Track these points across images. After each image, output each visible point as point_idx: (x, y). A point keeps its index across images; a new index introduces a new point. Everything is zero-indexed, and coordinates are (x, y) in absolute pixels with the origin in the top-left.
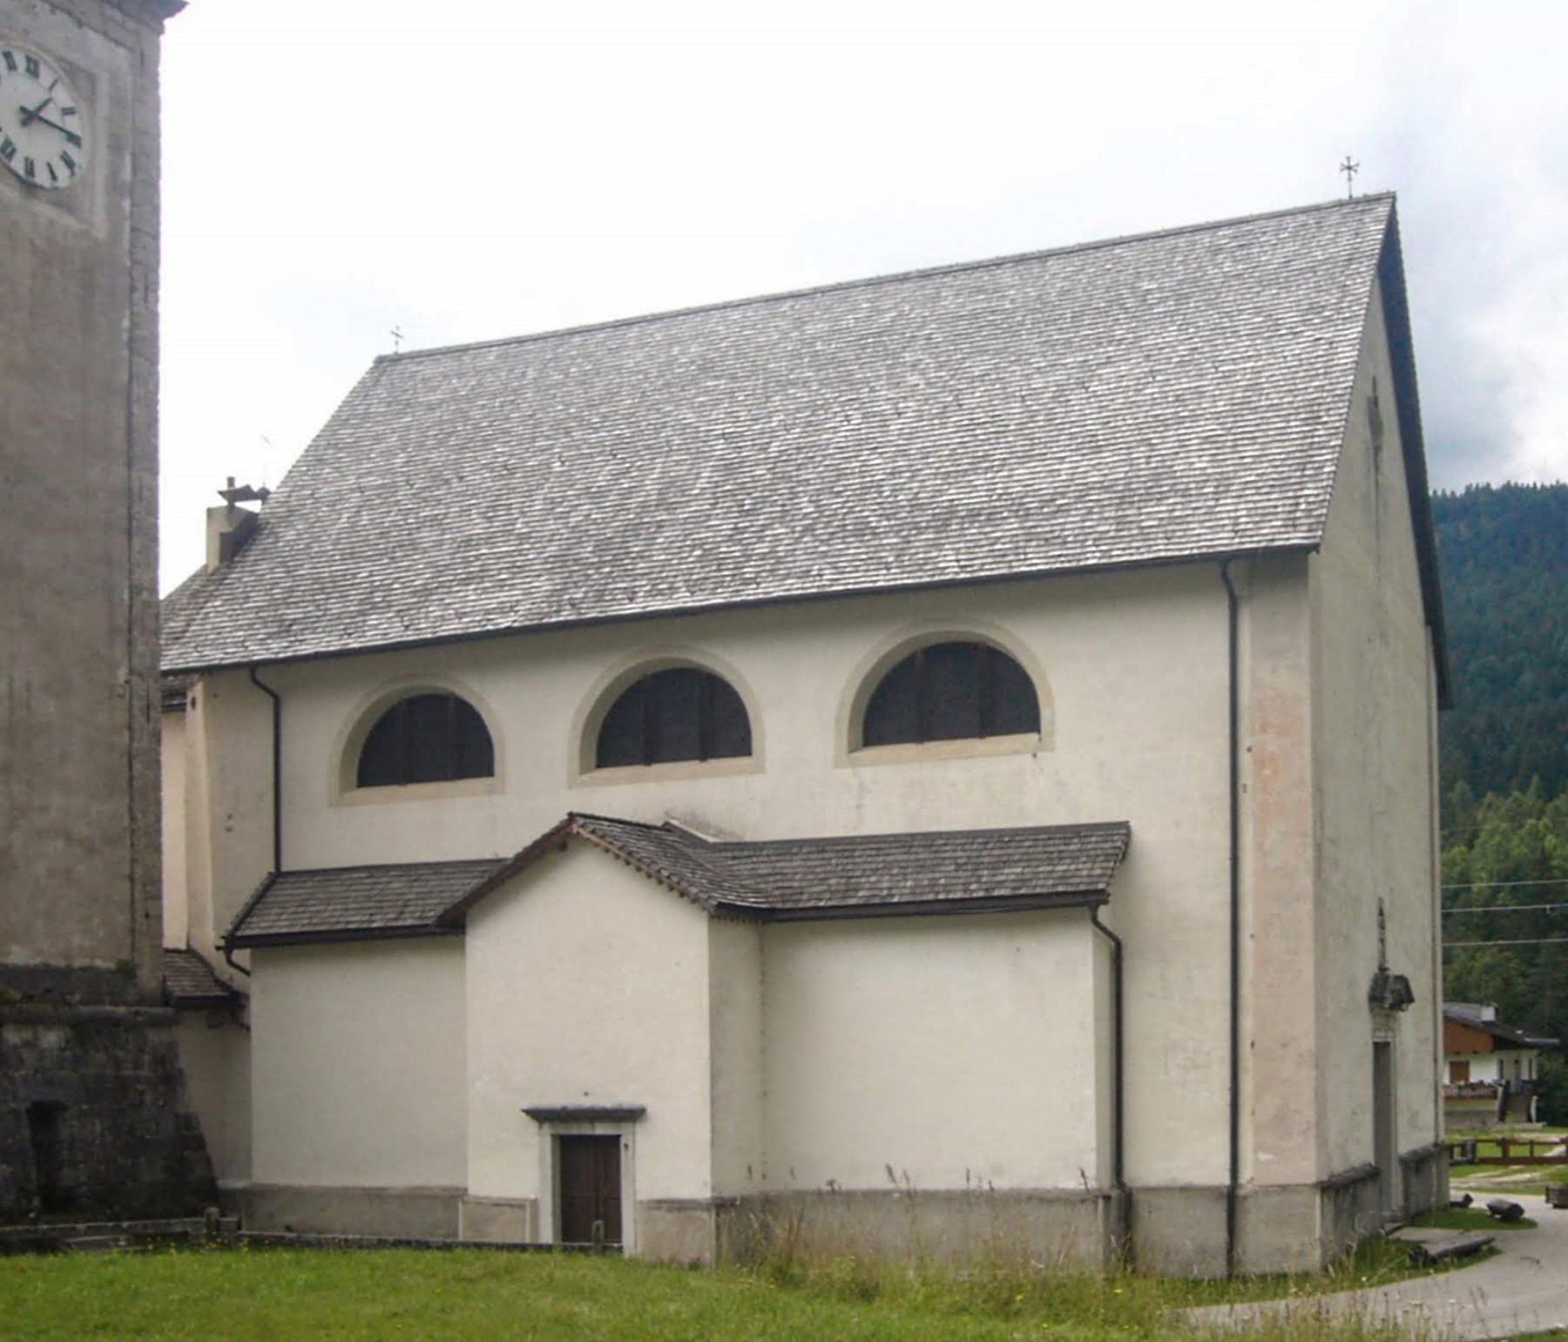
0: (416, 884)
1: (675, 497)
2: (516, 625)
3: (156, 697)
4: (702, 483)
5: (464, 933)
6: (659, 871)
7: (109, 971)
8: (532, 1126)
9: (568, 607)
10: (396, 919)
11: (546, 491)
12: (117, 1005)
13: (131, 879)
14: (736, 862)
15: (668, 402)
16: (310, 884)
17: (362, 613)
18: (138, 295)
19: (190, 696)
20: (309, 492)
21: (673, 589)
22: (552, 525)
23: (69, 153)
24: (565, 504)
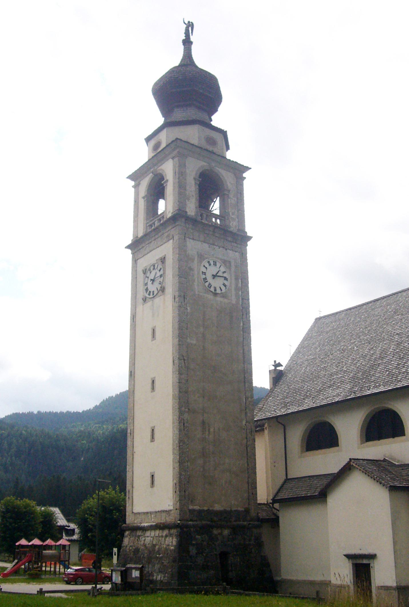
0: (320, 481)
1: (384, 355)
2: (340, 400)
3: (254, 428)
4: (391, 350)
5: (326, 497)
6: (374, 476)
7: (242, 511)
8: (346, 560)
9: (353, 393)
10: (313, 493)
11: (352, 356)
12: (244, 521)
13: (248, 483)
14: (403, 471)
15: (385, 324)
16: (294, 482)
17: (304, 399)
18: (244, 316)
19: (265, 426)
20: (295, 362)
21: (380, 385)
22: (353, 367)
23: (225, 282)
24: (356, 360)
